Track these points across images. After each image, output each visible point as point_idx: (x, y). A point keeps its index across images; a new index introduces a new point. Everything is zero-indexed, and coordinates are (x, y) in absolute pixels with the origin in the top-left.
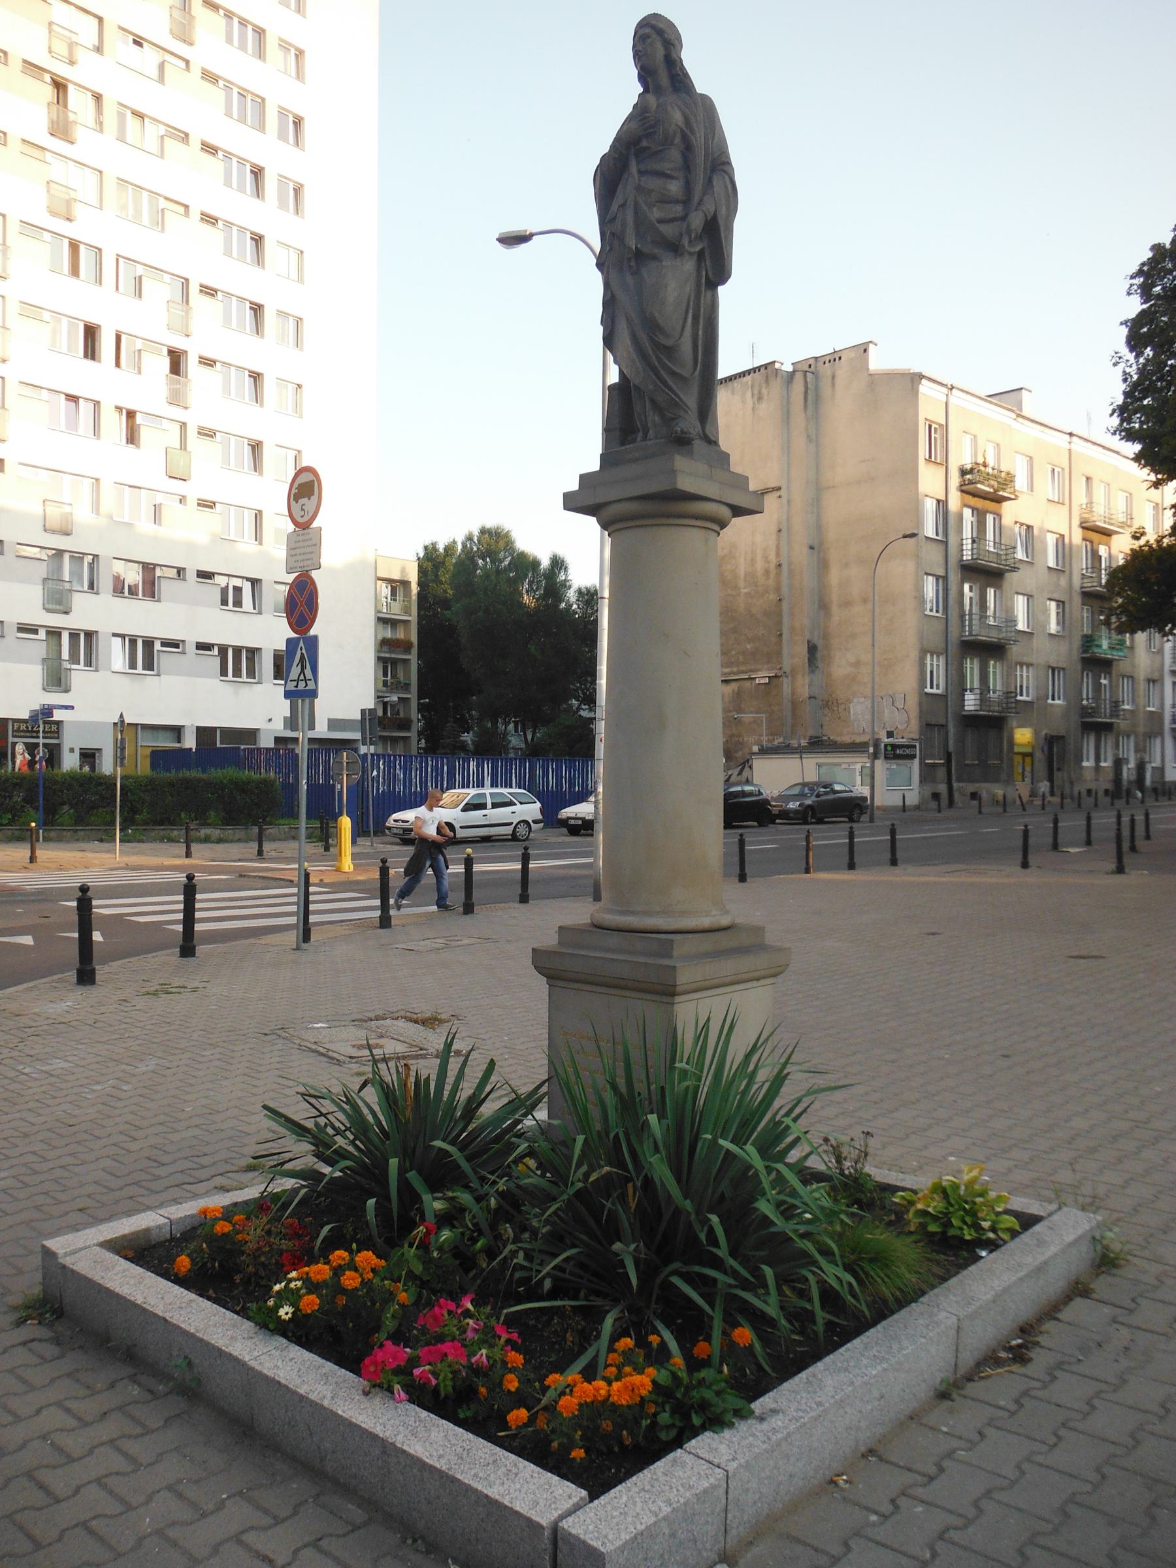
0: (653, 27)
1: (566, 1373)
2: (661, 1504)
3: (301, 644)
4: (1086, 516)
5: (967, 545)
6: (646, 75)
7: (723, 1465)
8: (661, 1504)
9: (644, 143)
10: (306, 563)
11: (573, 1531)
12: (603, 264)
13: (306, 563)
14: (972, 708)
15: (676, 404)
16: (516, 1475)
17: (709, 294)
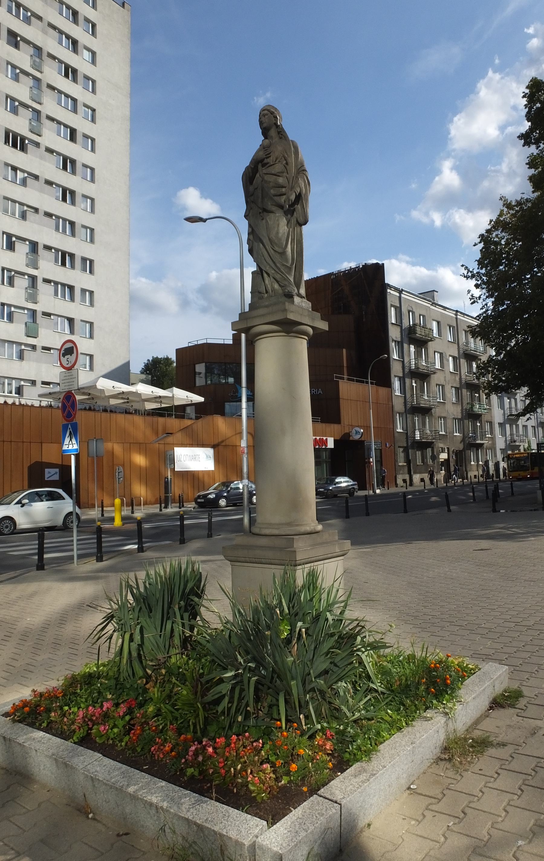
0: (268, 110)
1: (354, 547)
2: (309, 825)
3: (70, 426)
4: (465, 348)
5: (413, 362)
6: (265, 132)
7: (338, 801)
8: (309, 825)
9: (266, 161)
10: (70, 387)
11: (264, 843)
12: (248, 216)
13: (70, 387)
14: (419, 438)
15: (285, 279)
16: (229, 816)
17: (299, 228)
